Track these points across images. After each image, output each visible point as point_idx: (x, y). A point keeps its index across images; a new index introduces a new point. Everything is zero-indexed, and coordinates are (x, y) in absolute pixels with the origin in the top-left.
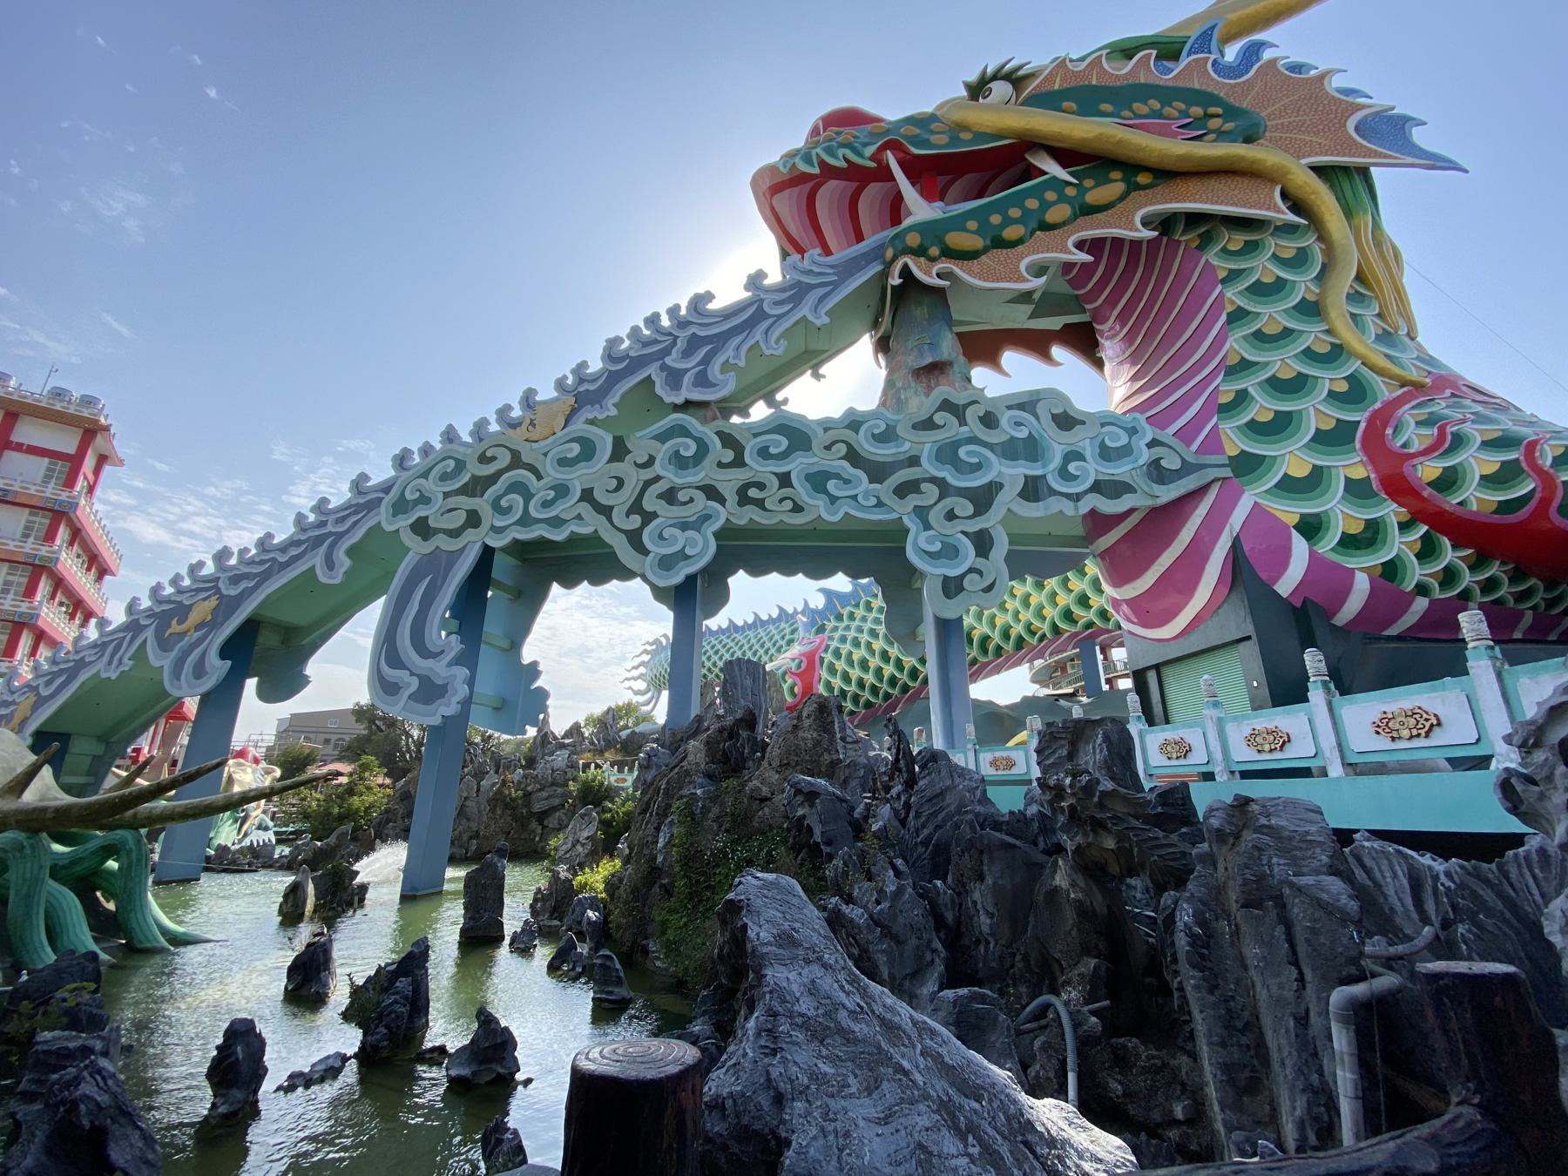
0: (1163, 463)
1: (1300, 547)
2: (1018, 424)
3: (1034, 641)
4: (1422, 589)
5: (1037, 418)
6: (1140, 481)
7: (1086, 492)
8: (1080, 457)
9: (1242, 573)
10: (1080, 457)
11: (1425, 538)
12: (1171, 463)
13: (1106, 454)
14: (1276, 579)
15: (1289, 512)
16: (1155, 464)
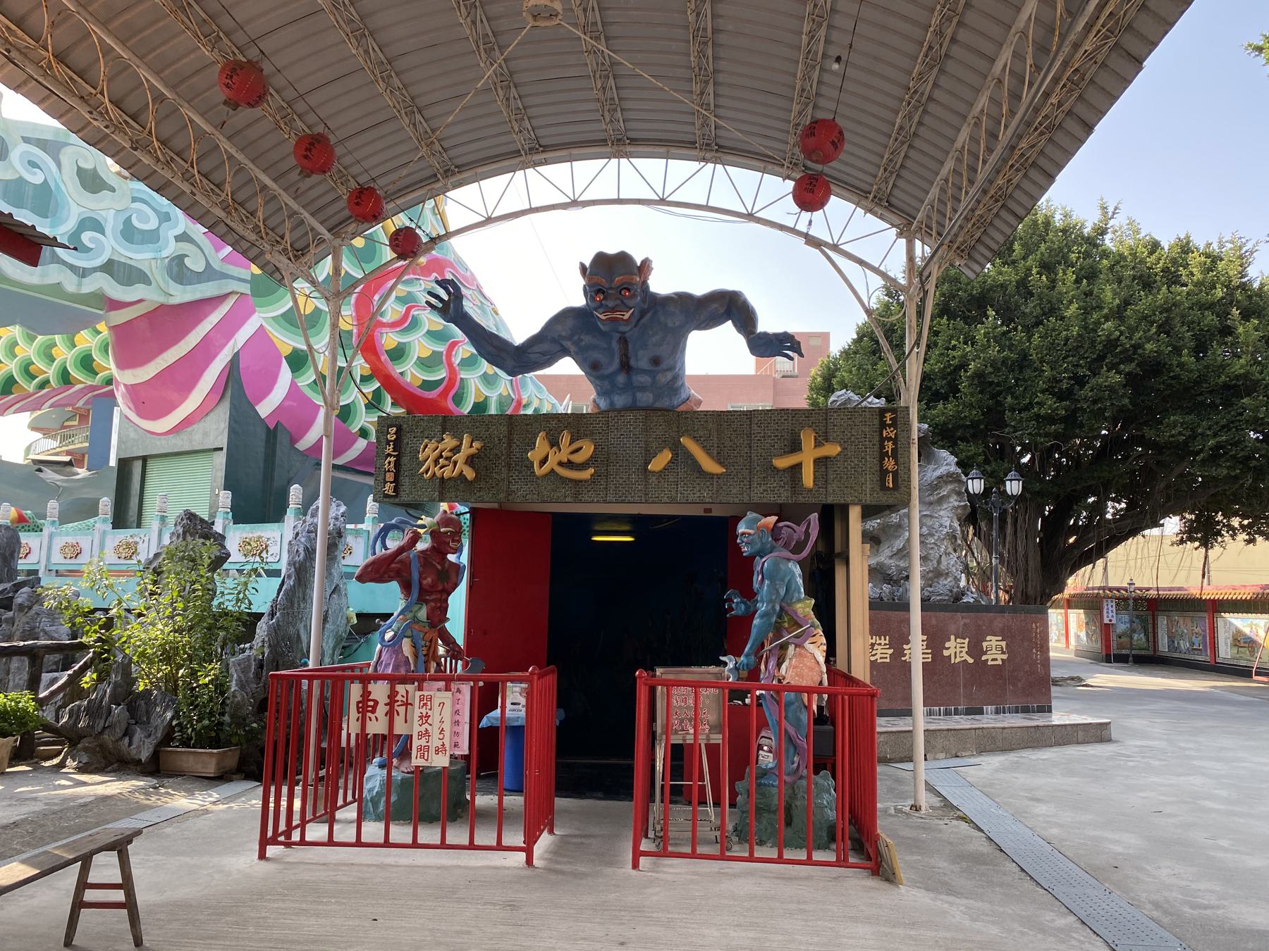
0: (187, 261)
1: (285, 374)
2: (33, 164)
3: (31, 387)
4: (363, 433)
5: (59, 165)
6: (158, 275)
7: (95, 270)
8: (98, 227)
9: (237, 388)
10: (98, 227)
11: (377, 393)
12: (195, 264)
13: (129, 233)
14: (260, 400)
15: (286, 341)
16: (179, 259)
